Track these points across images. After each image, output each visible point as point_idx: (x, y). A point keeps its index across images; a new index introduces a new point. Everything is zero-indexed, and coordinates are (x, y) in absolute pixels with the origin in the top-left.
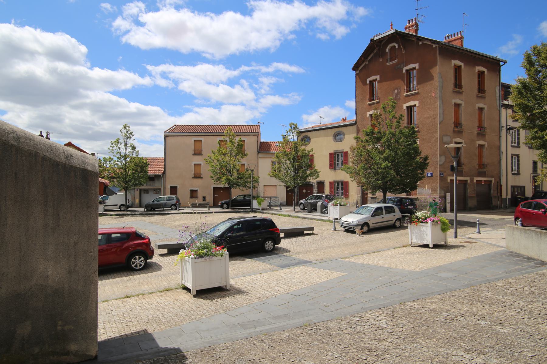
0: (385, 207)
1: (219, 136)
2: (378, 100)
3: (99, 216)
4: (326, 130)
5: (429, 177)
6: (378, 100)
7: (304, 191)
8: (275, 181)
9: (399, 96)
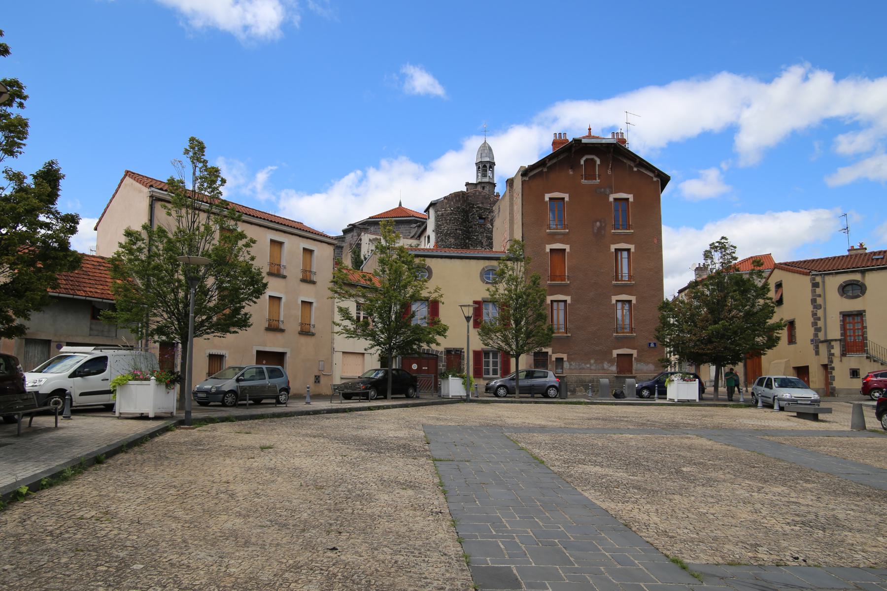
0: (35, 408)
1: (270, 230)
2: (568, 231)
3: (855, 406)
4: (467, 261)
5: (652, 347)
6: (568, 231)
7: (415, 367)
8: (361, 344)
9: (603, 232)
